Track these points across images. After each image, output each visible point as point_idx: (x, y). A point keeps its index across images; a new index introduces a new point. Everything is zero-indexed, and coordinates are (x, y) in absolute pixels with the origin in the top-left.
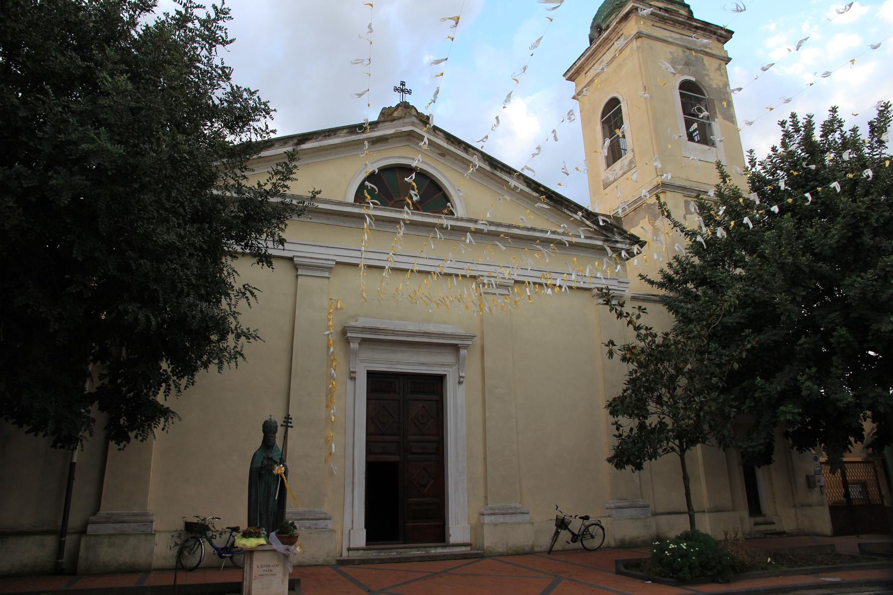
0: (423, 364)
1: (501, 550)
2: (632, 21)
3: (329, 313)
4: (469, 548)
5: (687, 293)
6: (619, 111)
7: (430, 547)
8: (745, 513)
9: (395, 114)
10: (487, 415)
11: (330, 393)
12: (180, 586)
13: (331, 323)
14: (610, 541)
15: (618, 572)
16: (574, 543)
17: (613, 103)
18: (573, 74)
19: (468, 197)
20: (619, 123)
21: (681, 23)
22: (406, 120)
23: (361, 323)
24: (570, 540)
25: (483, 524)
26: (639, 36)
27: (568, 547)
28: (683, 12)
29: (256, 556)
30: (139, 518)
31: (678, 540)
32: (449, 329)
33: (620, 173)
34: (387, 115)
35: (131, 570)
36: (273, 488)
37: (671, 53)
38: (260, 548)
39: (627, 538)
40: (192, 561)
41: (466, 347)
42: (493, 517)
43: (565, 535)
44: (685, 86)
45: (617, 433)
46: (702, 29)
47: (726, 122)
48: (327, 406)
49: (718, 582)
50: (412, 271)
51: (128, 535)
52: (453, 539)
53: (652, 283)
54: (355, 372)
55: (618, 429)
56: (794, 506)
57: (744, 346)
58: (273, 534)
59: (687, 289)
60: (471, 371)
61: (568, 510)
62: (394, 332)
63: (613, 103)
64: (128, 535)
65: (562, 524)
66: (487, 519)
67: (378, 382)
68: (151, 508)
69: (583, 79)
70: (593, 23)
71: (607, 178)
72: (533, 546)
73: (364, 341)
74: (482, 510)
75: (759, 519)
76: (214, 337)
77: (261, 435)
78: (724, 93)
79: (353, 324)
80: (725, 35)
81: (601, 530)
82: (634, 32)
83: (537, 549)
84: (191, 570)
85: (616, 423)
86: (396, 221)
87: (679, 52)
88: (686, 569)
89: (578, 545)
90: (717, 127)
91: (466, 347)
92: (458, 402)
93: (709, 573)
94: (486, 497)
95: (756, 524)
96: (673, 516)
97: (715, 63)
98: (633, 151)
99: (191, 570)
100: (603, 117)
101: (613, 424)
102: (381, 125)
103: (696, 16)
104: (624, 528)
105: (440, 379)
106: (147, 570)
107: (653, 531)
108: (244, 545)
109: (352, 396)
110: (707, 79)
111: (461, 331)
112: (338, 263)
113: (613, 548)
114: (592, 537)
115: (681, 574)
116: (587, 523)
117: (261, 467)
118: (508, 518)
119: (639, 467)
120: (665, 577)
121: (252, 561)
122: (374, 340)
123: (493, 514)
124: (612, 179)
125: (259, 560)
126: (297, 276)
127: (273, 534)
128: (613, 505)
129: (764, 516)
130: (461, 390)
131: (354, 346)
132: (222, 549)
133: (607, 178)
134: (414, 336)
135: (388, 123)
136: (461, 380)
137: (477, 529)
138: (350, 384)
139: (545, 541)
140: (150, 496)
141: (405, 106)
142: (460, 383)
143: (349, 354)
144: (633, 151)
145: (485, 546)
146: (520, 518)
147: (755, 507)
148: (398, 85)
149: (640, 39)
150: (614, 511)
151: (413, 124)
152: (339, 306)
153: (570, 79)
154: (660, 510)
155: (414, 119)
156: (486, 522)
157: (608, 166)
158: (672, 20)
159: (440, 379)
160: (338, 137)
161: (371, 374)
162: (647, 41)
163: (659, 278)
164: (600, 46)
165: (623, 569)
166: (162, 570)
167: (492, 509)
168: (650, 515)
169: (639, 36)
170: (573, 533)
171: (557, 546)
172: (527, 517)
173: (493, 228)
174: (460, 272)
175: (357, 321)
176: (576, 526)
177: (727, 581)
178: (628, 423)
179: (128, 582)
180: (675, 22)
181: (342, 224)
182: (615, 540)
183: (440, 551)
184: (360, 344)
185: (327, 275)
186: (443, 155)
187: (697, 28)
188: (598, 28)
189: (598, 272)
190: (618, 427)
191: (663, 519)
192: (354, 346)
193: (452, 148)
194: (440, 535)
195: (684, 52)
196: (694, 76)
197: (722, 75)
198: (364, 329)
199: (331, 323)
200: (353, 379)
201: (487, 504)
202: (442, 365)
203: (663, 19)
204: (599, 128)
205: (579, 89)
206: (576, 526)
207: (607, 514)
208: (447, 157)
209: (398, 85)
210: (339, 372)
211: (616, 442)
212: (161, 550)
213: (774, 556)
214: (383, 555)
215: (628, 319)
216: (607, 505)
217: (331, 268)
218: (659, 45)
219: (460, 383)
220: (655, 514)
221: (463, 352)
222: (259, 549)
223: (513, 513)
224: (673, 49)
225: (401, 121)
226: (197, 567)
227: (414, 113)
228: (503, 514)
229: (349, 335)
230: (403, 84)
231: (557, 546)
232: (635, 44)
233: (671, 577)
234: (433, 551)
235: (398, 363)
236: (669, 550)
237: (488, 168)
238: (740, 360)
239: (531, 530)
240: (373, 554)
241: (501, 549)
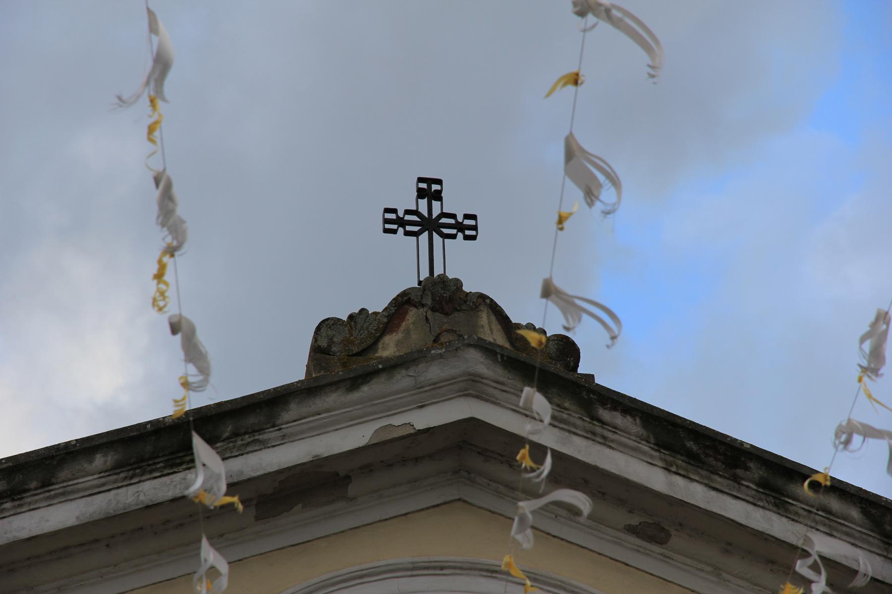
141: (442, 302)
148: (406, 199)
151: (471, 386)
160: (66, 496)
193: (695, 493)
208: (677, 541)
209: (406, 199)
230: (429, 189)
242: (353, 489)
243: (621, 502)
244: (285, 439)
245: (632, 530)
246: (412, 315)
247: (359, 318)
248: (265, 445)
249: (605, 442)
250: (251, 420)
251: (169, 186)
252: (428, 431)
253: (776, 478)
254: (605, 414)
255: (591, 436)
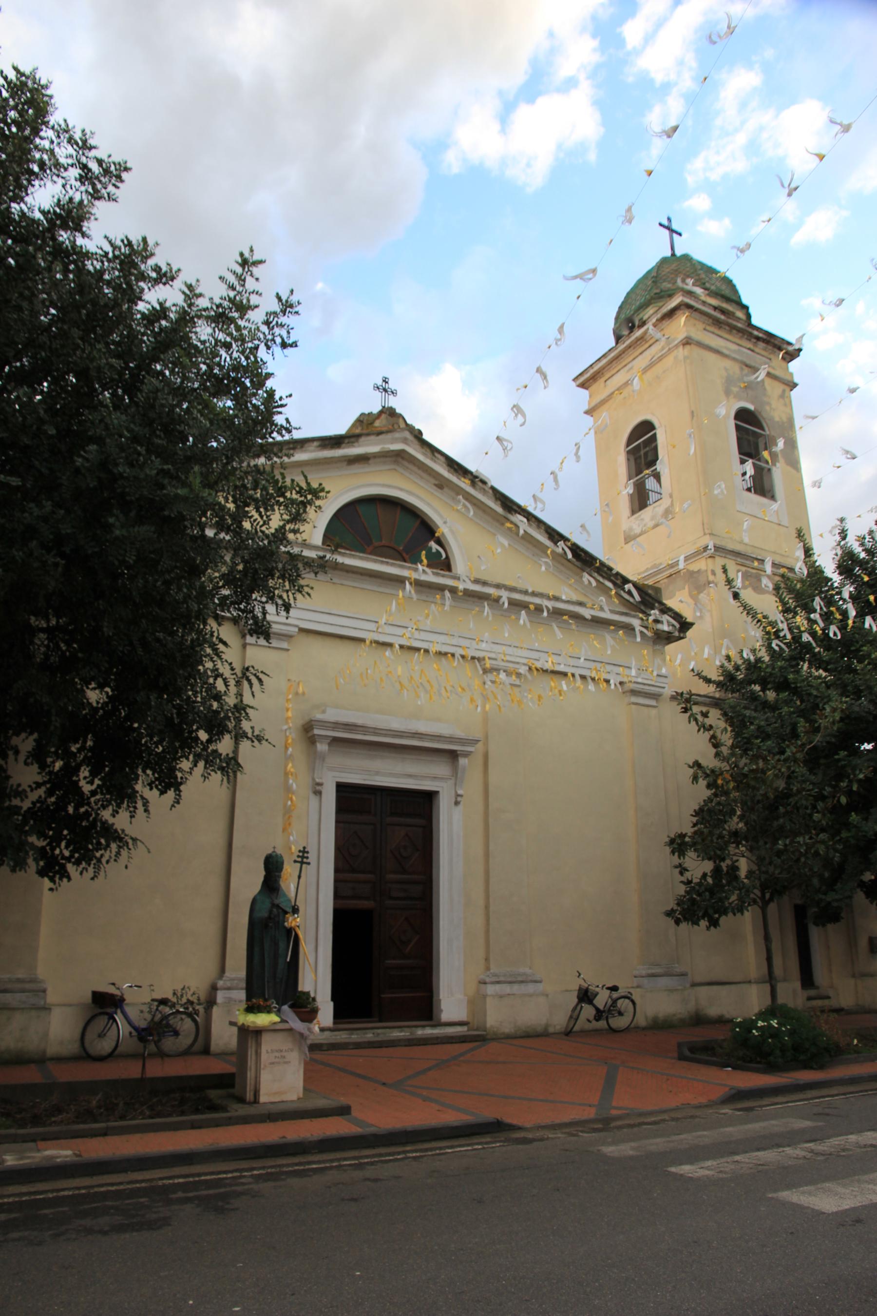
0: (410, 776)
1: (507, 1031)
2: (682, 319)
3: (288, 700)
4: (465, 1028)
5: (754, 697)
6: (654, 438)
7: (416, 1026)
8: (798, 984)
9: (377, 423)
10: (490, 848)
11: (288, 813)
12: (152, 1079)
13: (290, 714)
14: (641, 1021)
15: (682, 1058)
16: (599, 1023)
17: (645, 428)
18: (588, 380)
19: (474, 549)
20: (652, 460)
21: (739, 330)
22: (397, 435)
23: (331, 715)
24: (591, 1018)
25: (485, 997)
26: (687, 342)
27: (588, 1026)
28: (740, 314)
29: (266, 1038)
30: (27, 986)
31: (762, 1015)
32: (444, 729)
33: (651, 524)
34: (365, 425)
35: (19, 1060)
36: (282, 945)
37: (726, 370)
38: (273, 1028)
39: (661, 1015)
40: (105, 1046)
41: (467, 754)
42: (498, 987)
43: (588, 1011)
44: (743, 415)
45: (683, 879)
46: (764, 341)
47: (789, 469)
48: (284, 830)
49: (812, 1068)
50: (427, 651)
51: (14, 1009)
52: (445, 1017)
53: (708, 681)
54: (321, 784)
55: (681, 873)
56: (854, 976)
57: (855, 775)
58: (285, 1008)
59: (753, 693)
60: (471, 787)
61: (595, 980)
62: (376, 731)
63: (645, 428)
64: (14, 1009)
65: (585, 996)
66: (491, 989)
67: (352, 799)
68: (41, 972)
69: (602, 389)
70: (619, 313)
71: (631, 529)
72: (547, 1026)
73: (335, 741)
74: (482, 977)
75: (812, 992)
76: (203, 736)
77: (261, 874)
78: (788, 427)
79: (319, 716)
80: (793, 354)
81: (631, 1004)
82: (681, 336)
83: (551, 1030)
84: (101, 1059)
85: (680, 865)
86: (400, 581)
87: (735, 369)
88: (778, 1052)
89: (602, 1024)
90: (779, 474)
91: (467, 754)
92: (454, 829)
93: (802, 1057)
94: (487, 960)
95: (809, 999)
96: (715, 988)
97: (779, 388)
98: (671, 496)
99: (101, 1059)
100: (628, 444)
101: (676, 867)
102: (363, 439)
103: (755, 321)
104: (658, 1002)
105: (428, 798)
106: (40, 1060)
107: (691, 1007)
108: (253, 1022)
109: (316, 817)
110: (768, 408)
111: (459, 733)
112: (302, 630)
113: (644, 1029)
114: (621, 1014)
115: (771, 1058)
116: (615, 995)
117: (270, 918)
118: (516, 989)
119: (714, 923)
120: (751, 1061)
121: (259, 1045)
122: (351, 741)
123: (498, 982)
124: (637, 530)
125: (268, 1044)
126: (244, 646)
127: (285, 1008)
128: (644, 973)
129: (817, 988)
130: (458, 812)
131: (322, 747)
132: (144, 1030)
133: (631, 529)
134: (401, 737)
135: (373, 438)
136: (459, 799)
137: (477, 1002)
138: (314, 800)
139: (560, 1021)
140: (41, 954)
141: (390, 413)
142: (457, 803)
143: (314, 759)
144: (671, 496)
145: (488, 1025)
146: (531, 988)
147: (807, 979)
148: (380, 382)
149: (688, 347)
150: (645, 981)
151: (405, 441)
152: (301, 690)
153: (583, 385)
154: (698, 979)
155: (407, 434)
156: (489, 993)
157: (633, 512)
158: (729, 325)
159: (428, 798)
160: (305, 451)
161: (342, 788)
162: (697, 351)
163: (714, 676)
164: (629, 347)
165: (687, 1053)
166: (59, 1059)
167: (495, 975)
168: (688, 985)
169: (687, 342)
170: (597, 1009)
171: (576, 1028)
172: (540, 987)
173: (477, 588)
174: (459, 652)
175: (324, 712)
176: (602, 1000)
177: (821, 1067)
178: (699, 867)
179: (29, 1075)
180: (732, 328)
181: (375, 588)
182: (646, 1018)
183: (429, 1031)
184: (330, 744)
185: (285, 645)
186: (440, 487)
187: (758, 339)
188: (628, 323)
189: (636, 664)
190: (683, 870)
191: (704, 991)
192: (322, 747)
193: (454, 478)
194: (424, 1007)
195: (742, 369)
196: (752, 403)
197: (785, 405)
198: (336, 725)
199: (290, 714)
200: (318, 793)
201: (488, 969)
202: (435, 778)
203: (717, 323)
204: (621, 459)
205: (593, 404)
206: (602, 1000)
207: (635, 985)
208: (446, 489)
209: (380, 382)
210: (299, 784)
211: (682, 890)
212: (59, 1030)
213: (862, 1038)
214: (355, 1037)
215: (711, 732)
216: (636, 973)
217: (291, 636)
218: (711, 357)
219: (457, 803)
220: (694, 985)
221: (462, 761)
222: (272, 1029)
223: (522, 982)
224: (728, 363)
225: (389, 436)
226: (111, 1055)
227: (402, 425)
228: (510, 982)
229: (316, 732)
230: (385, 381)
231: (576, 1028)
232: (681, 352)
233: (759, 1063)
234: (420, 1032)
235: (377, 773)
236: (757, 1028)
237: (499, 509)
238: (849, 793)
239: (544, 1004)
240: (342, 1037)
241: (507, 1029)
242: (371, 461)
243: (434, 477)
244: (359, 446)
245: (436, 485)
246: (383, 416)
247: (370, 414)
248: (354, 446)
249: (435, 462)
250: (352, 440)
251: (579, 448)
252: (393, 451)
253: (475, 479)
254: (436, 454)
255: (432, 459)
